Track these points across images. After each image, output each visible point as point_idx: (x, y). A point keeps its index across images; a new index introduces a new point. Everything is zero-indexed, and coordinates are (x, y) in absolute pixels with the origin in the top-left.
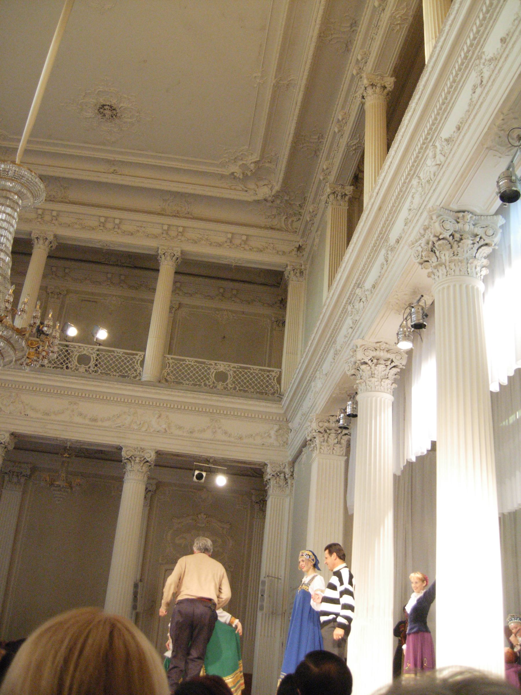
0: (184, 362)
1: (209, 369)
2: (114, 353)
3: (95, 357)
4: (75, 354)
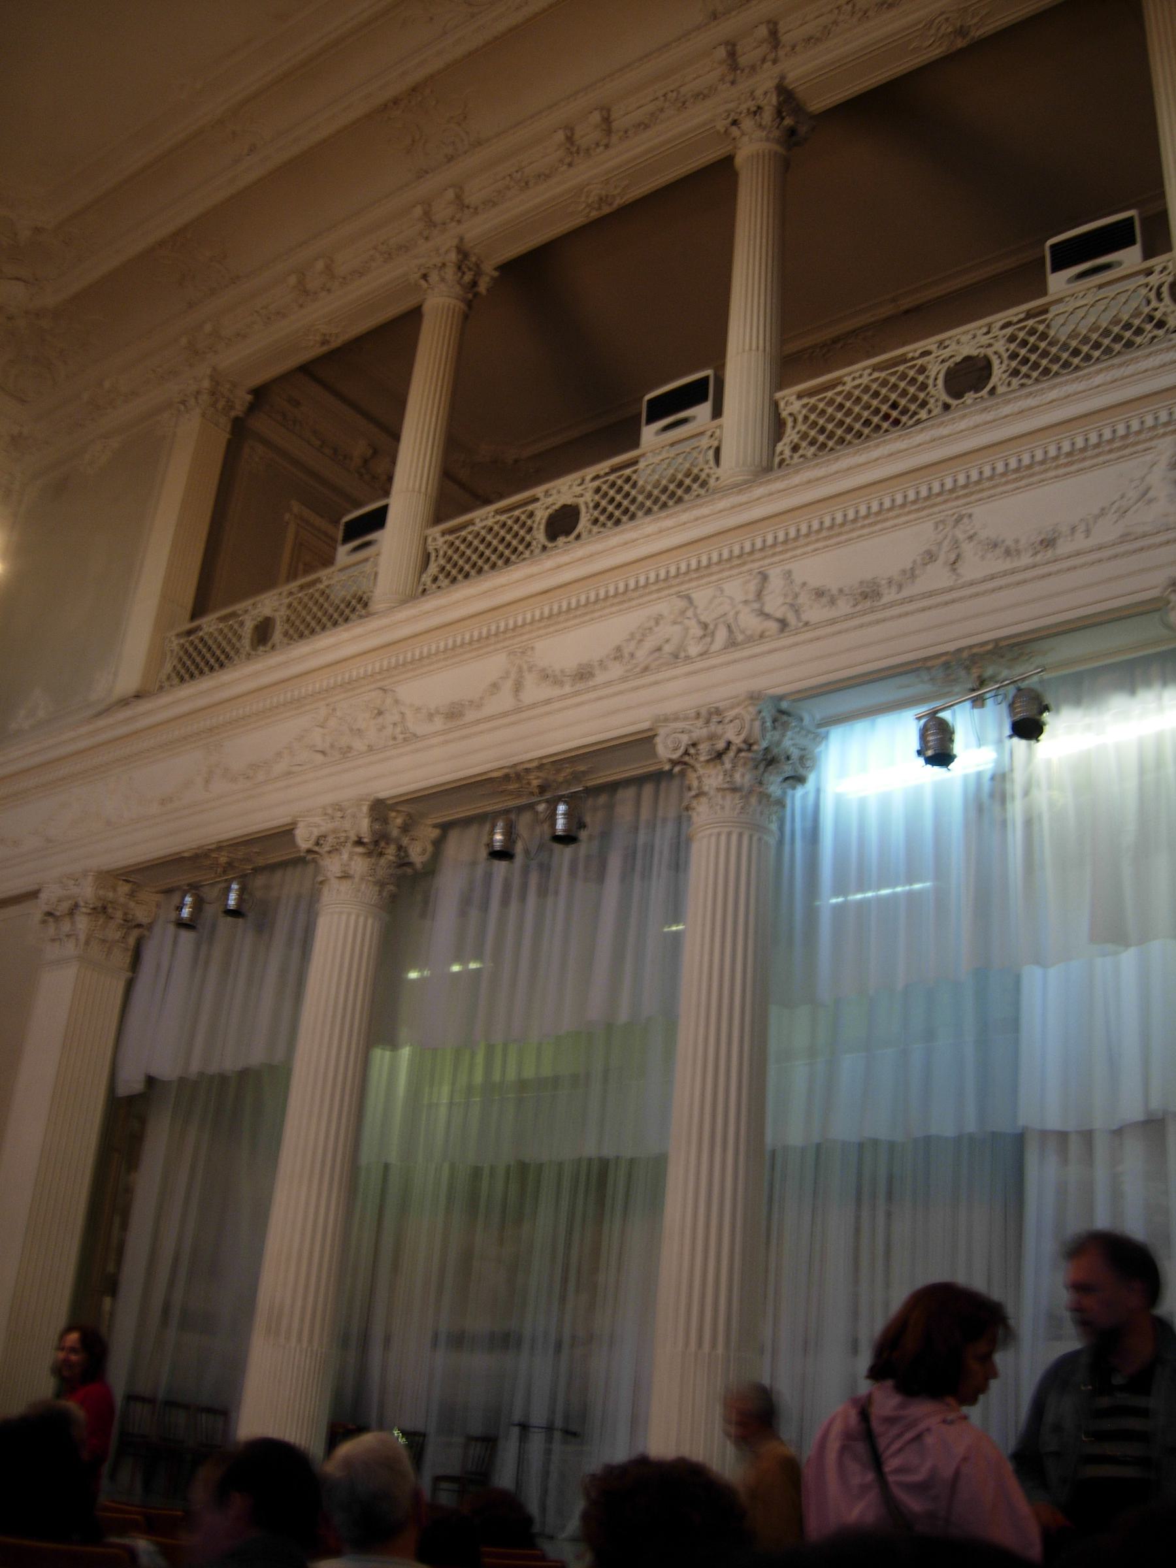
0: (839, 389)
1: (922, 370)
2: (473, 524)
3: (1002, 350)
4: (933, 374)
